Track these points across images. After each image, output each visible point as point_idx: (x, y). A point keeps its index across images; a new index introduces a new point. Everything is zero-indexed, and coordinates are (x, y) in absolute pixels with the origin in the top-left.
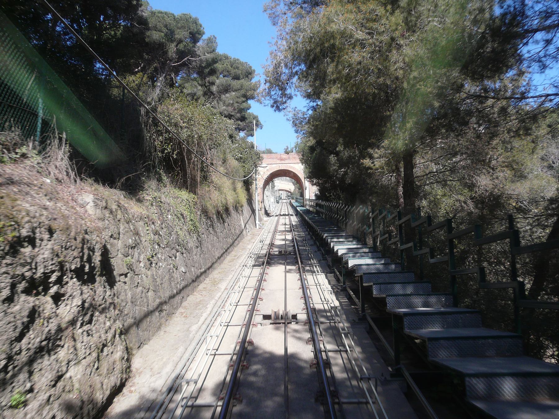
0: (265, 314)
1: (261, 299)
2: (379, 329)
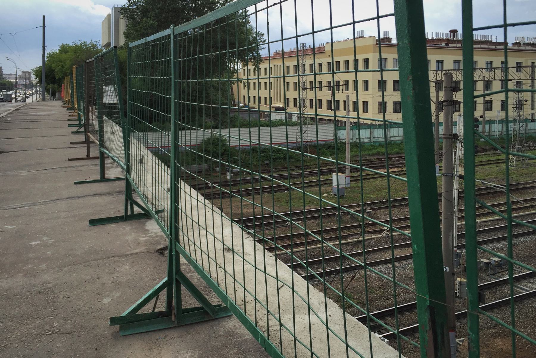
0: (359, 60)
2: (356, 167)
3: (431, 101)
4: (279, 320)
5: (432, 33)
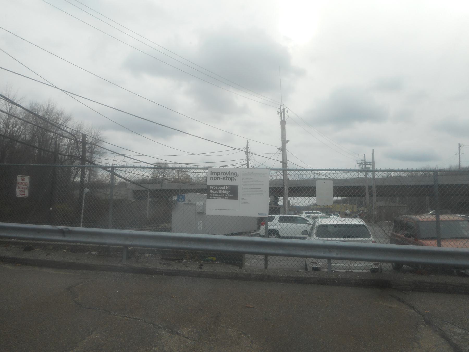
0: (440, 247)
5: (261, 189)
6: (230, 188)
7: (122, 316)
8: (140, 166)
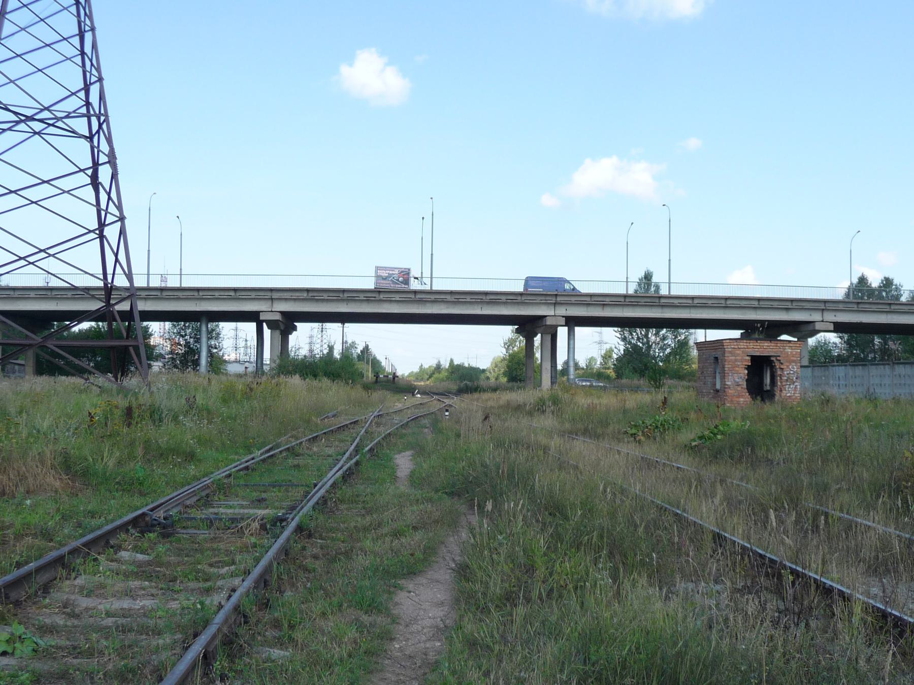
0: (378, 265)
1: (452, 361)
3: (79, 49)
4: (116, 251)
6: (94, 306)
7: (162, 589)
8: (91, 186)
